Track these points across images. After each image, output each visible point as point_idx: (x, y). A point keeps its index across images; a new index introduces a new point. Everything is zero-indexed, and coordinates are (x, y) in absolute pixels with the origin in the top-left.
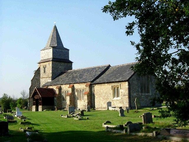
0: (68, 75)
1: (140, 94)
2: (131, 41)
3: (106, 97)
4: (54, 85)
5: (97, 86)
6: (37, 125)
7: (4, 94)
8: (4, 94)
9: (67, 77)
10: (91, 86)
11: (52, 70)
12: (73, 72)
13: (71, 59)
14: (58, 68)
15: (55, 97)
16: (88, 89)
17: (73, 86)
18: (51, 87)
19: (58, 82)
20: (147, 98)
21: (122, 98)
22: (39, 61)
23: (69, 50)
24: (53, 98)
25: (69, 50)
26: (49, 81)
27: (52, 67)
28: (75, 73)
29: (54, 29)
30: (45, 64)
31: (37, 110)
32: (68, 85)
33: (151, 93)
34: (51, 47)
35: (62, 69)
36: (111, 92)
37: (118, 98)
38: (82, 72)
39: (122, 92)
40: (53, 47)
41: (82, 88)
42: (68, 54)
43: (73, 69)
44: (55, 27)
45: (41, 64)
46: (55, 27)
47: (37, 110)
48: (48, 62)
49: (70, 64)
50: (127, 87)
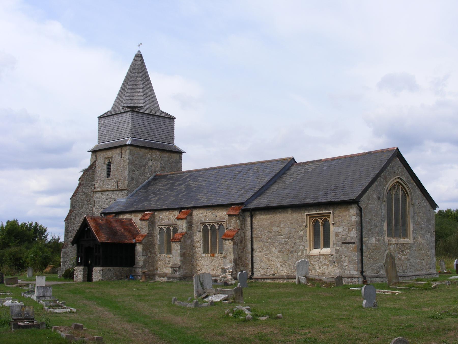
0: (173, 184)
1: (386, 239)
2: (141, 44)
3: (288, 247)
6: (427, 275)
9: (171, 189)
12: (188, 177)
13: (179, 143)
14: (145, 166)
19: (146, 203)
20: (402, 251)
21: (337, 251)
25: (172, 119)
28: (194, 180)
30: (109, 154)
31: (88, 277)
32: (177, 213)
33: (412, 238)
36: (308, 233)
37: (326, 251)
39: (337, 234)
41: (218, 218)
42: (334, 159)
47: (88, 277)
49: (176, 156)
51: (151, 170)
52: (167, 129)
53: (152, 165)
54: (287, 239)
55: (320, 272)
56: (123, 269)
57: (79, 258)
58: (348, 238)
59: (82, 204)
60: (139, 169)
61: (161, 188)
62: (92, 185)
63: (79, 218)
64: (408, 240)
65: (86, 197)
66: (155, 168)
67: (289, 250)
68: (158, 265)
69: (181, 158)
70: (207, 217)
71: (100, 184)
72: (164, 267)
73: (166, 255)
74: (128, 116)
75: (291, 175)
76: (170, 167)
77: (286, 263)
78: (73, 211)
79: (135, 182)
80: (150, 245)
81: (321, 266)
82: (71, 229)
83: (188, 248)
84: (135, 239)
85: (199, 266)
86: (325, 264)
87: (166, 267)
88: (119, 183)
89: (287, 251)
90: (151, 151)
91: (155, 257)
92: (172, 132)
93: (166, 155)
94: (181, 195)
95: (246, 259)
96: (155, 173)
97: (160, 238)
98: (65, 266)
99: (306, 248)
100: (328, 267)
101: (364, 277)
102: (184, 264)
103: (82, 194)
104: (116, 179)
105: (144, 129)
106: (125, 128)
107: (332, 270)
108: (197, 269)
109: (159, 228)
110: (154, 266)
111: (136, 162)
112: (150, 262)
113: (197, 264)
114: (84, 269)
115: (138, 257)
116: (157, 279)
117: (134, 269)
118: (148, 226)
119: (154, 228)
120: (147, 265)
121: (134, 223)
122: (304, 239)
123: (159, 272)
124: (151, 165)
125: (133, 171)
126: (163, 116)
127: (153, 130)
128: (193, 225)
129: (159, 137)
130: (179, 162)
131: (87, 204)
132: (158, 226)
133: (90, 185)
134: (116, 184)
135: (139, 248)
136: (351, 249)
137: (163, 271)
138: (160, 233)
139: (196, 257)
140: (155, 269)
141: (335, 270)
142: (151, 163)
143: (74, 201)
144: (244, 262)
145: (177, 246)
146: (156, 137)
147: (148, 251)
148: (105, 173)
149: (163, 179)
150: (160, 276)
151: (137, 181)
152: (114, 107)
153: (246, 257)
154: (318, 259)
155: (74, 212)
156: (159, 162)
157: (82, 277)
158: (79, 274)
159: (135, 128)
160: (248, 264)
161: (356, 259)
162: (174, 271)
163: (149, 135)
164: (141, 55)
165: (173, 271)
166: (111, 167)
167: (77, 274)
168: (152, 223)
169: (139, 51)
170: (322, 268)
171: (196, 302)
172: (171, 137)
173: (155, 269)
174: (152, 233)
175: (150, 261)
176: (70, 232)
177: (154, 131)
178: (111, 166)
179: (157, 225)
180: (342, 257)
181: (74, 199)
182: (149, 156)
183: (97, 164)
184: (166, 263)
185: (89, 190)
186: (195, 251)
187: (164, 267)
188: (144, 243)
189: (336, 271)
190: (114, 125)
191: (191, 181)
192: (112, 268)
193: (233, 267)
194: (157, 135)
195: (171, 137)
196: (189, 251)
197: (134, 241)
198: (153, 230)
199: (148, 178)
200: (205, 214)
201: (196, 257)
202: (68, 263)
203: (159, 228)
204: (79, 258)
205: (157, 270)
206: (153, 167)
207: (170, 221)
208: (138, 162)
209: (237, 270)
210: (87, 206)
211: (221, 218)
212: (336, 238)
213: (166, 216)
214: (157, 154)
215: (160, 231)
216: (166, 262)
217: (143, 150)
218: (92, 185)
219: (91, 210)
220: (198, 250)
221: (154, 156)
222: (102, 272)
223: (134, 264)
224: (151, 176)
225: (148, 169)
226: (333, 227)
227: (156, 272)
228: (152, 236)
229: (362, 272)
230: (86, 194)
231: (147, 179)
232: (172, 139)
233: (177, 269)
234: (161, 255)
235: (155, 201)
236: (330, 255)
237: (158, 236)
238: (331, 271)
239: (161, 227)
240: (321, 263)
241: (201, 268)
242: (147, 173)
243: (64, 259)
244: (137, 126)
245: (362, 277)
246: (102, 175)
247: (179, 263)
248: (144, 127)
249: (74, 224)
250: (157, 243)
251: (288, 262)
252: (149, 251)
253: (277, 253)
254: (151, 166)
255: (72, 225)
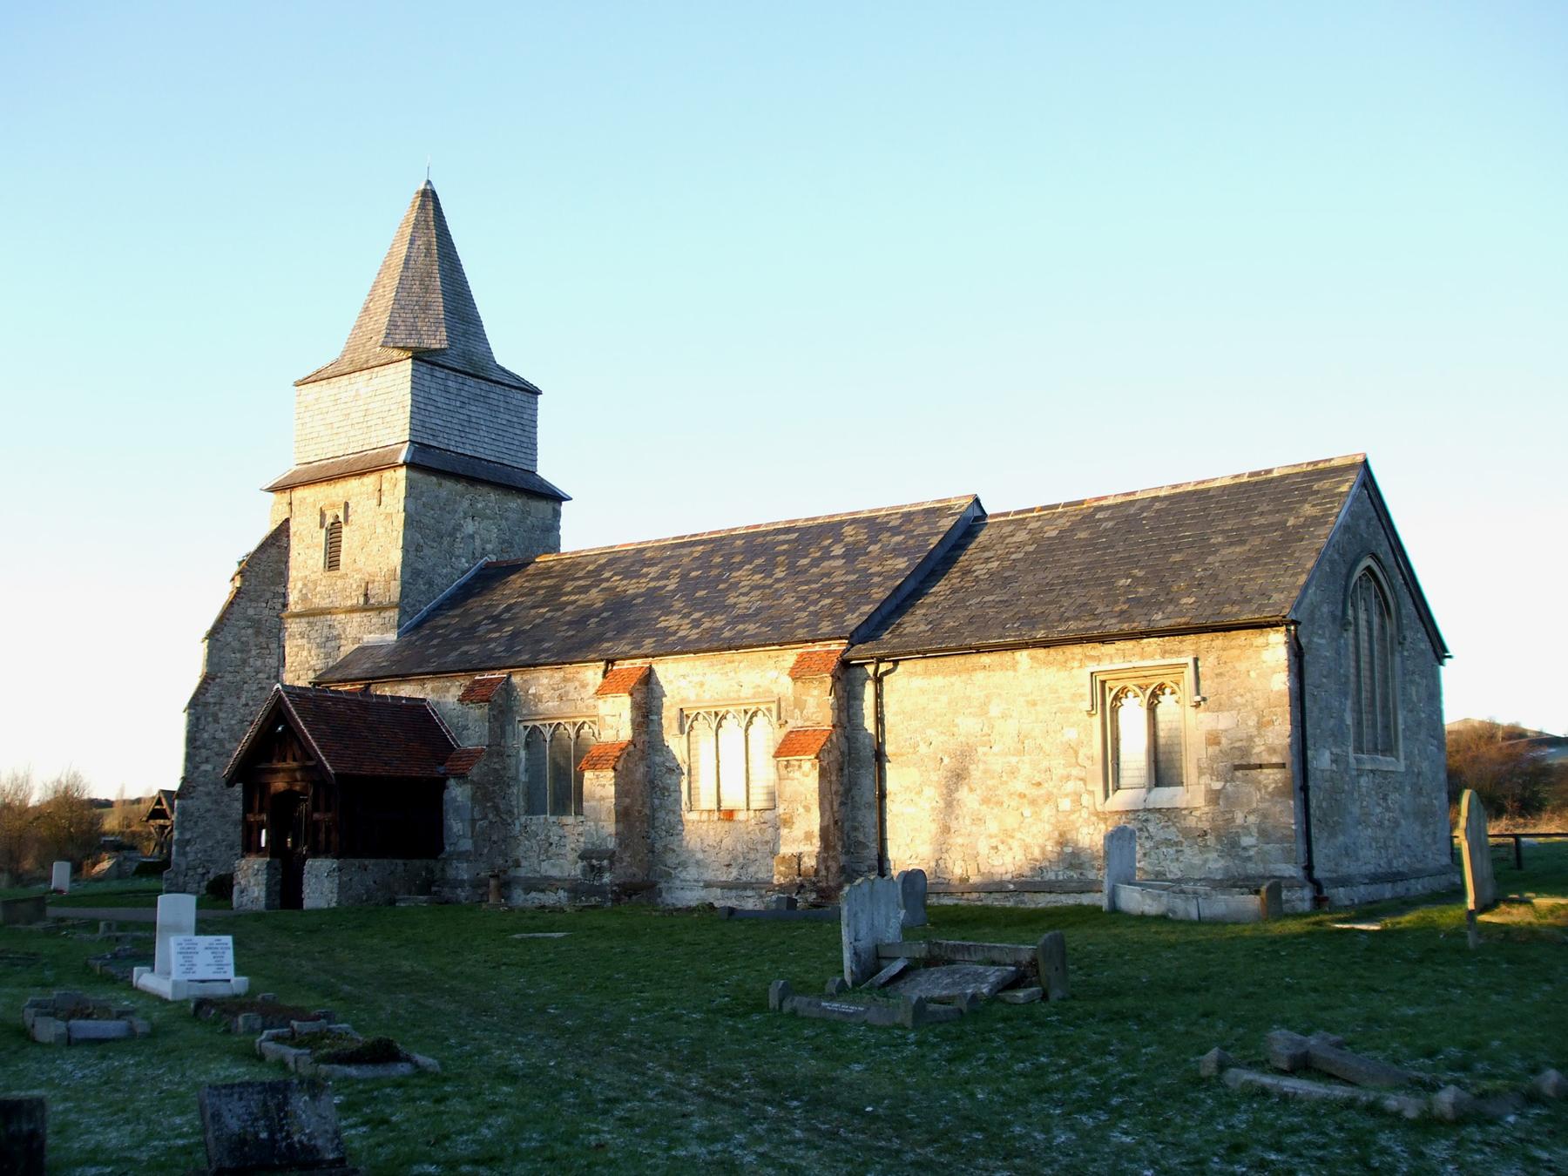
3: (1020, 786)
4: (437, 673)
5: (918, 682)
7: (75, 776)
8: (75, 776)
10: (846, 677)
11: (405, 549)
13: (549, 468)
14: (452, 535)
15: (462, 777)
16: (818, 706)
17: (648, 678)
18: (407, 691)
20: (1385, 798)
22: (284, 468)
23: (535, 392)
24: (440, 785)
25: (535, 392)
26: (371, 638)
27: (410, 523)
28: (628, 574)
29: (422, 207)
34: (395, 354)
35: (485, 541)
38: (704, 562)
40: (420, 357)
41: (746, 692)
43: (563, 550)
44: (429, 197)
45: (299, 494)
46: (429, 197)
48: (371, 480)
49: (543, 507)
50: (1280, 682)
51: (471, 550)
52: (516, 425)
53: (475, 533)
54: (1013, 755)
55: (1149, 868)
56: (405, 865)
57: (264, 832)
58: (1257, 750)
59: (244, 656)
60: (435, 545)
61: (516, 603)
62: (275, 595)
63: (234, 700)
64: (1394, 759)
65: (257, 633)
66: (485, 541)
67: (1022, 796)
68: (519, 853)
69: (557, 515)
70: (706, 687)
71: (304, 592)
72: (541, 857)
73: (553, 819)
74: (402, 375)
75: (985, 549)
76: (527, 543)
77: (1013, 837)
78: (213, 679)
79: (424, 585)
80: (495, 784)
81: (1151, 848)
82: (206, 736)
83: (638, 791)
84: (442, 764)
85: (674, 851)
86: (1168, 842)
87: (549, 858)
88: (370, 586)
89: (1017, 798)
90: (470, 488)
91: (509, 825)
92: (531, 435)
93: (515, 503)
94: (597, 620)
95: (855, 829)
96: (481, 558)
97: (527, 759)
98: (185, 854)
99: (1090, 788)
100: (1177, 851)
101: (1317, 885)
102: (627, 846)
103: (242, 623)
104: (359, 576)
105: (449, 419)
106: (391, 413)
107: (1197, 861)
108: (669, 863)
109: (526, 727)
110: (506, 855)
111: (426, 521)
112: (495, 842)
113: (665, 846)
114: (269, 864)
115: (454, 825)
116: (519, 897)
117: (440, 865)
118: (489, 722)
119: (509, 728)
120: (486, 851)
121: (434, 712)
122: (1081, 755)
123: (522, 872)
124: (471, 532)
125: (417, 550)
126: (507, 382)
127: (476, 426)
128: (651, 717)
129: (494, 447)
130: (551, 529)
131: (259, 656)
132: (520, 721)
133: (269, 595)
134: (362, 590)
135: (457, 793)
136: (1270, 789)
137: (538, 872)
138: (527, 745)
139: (664, 824)
140: (510, 863)
141: (1206, 861)
142: (470, 527)
143: (219, 644)
144: (849, 837)
145: (604, 786)
146: (485, 446)
147: (489, 805)
148: (319, 557)
149: (512, 577)
150: (532, 886)
151: (430, 583)
152: (351, 348)
153: (854, 819)
154: (1140, 826)
155: (218, 680)
156: (494, 524)
157: (263, 894)
158: (252, 884)
159: (423, 412)
160: (860, 843)
161: (1293, 821)
162: (592, 871)
163: (464, 440)
164: (434, 193)
165: (588, 869)
166: (343, 539)
167: (243, 882)
168: (501, 712)
169: (429, 182)
170: (1154, 856)
171: (784, 985)
172: (528, 451)
173: (510, 863)
174: (499, 745)
175: (495, 838)
176: (204, 746)
177: (480, 427)
178: (343, 535)
179: (519, 719)
180: (1233, 818)
181: (217, 640)
182: (466, 504)
183: (292, 530)
184: (551, 844)
185: (266, 612)
186: (661, 804)
187: (541, 857)
188: (475, 779)
189: (1211, 865)
190: (349, 405)
191: (618, 578)
192: (373, 861)
193: (819, 853)
194: (486, 440)
195: (528, 451)
196: (641, 802)
197: (441, 769)
198: (503, 734)
199: (464, 573)
200: (697, 679)
201: (664, 824)
202: (197, 846)
203: (526, 727)
204: (264, 832)
205: (517, 864)
206: (478, 542)
207: (568, 703)
208: (432, 521)
209: (830, 863)
210: (259, 663)
211: (761, 690)
212: (1210, 750)
213: (553, 689)
214: (490, 499)
215: (528, 736)
216: (551, 840)
217: (449, 484)
218: (275, 595)
219: (272, 675)
220: (671, 799)
221: (479, 506)
222: (340, 877)
223: (442, 849)
224: (470, 568)
225: (462, 545)
226: (1197, 713)
227: (512, 873)
228: (500, 754)
229: (1309, 868)
230: (256, 625)
231: (459, 578)
232: (530, 457)
233: (605, 863)
234: (534, 817)
235: (502, 641)
236: (1185, 809)
237: (523, 753)
238: (1192, 866)
239: (535, 726)
240: (1150, 837)
241: (683, 858)
242: (458, 557)
243: (181, 833)
244: (429, 408)
245: (1310, 885)
246: (310, 562)
247: (611, 844)
248: (450, 414)
249: (216, 721)
250: (516, 779)
251: (1018, 835)
252: (492, 806)
253: (976, 806)
254: (472, 537)
255: (208, 723)
